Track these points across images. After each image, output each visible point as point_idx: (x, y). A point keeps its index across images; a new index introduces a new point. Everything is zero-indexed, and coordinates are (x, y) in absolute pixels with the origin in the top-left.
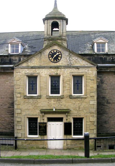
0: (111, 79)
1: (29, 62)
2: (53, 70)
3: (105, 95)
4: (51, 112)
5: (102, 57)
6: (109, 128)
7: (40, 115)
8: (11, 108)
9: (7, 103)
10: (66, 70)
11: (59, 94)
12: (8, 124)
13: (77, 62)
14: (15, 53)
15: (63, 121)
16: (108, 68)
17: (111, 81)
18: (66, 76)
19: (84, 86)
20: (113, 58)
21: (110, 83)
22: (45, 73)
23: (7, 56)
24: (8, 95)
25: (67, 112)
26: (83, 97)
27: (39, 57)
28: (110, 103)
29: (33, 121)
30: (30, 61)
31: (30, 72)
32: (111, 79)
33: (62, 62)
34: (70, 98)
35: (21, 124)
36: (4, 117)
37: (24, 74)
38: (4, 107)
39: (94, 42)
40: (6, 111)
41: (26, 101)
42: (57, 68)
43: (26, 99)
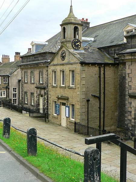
33: (66, 61)
42: (63, 65)
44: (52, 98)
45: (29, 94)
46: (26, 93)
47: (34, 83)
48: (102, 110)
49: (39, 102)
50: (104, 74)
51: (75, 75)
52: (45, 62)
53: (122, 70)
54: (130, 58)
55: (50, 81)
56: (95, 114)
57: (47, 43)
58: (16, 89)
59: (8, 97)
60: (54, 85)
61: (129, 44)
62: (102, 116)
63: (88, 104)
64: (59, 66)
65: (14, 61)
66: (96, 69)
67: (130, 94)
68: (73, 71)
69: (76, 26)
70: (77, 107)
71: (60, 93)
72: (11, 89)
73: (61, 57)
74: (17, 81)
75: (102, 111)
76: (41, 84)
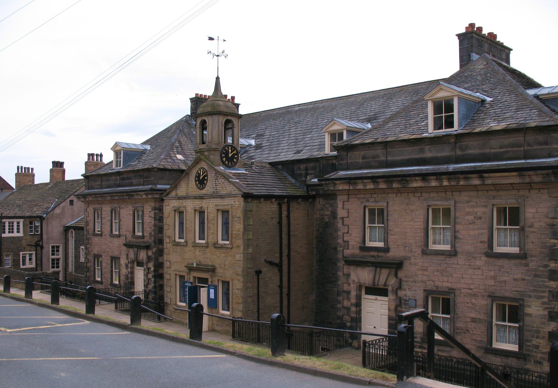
33: (209, 188)
34: (216, 247)
42: (201, 198)
44: (173, 269)
45: (106, 261)
46: (97, 257)
47: (119, 236)
48: (285, 291)
49: (133, 278)
50: (288, 217)
51: (230, 220)
52: (152, 190)
53: (322, 210)
54: (346, 187)
55: (168, 232)
56: (271, 299)
57: (148, 147)
58: (58, 247)
59: (39, 268)
60: (178, 240)
61: (343, 160)
62: (285, 302)
63: (258, 279)
64: (192, 200)
65: (48, 181)
66: (273, 207)
67: (345, 257)
68: (225, 213)
69: (229, 118)
70: (237, 286)
71: (194, 257)
72: (47, 249)
73: (196, 181)
74: (61, 229)
75: (285, 292)
76: (139, 237)
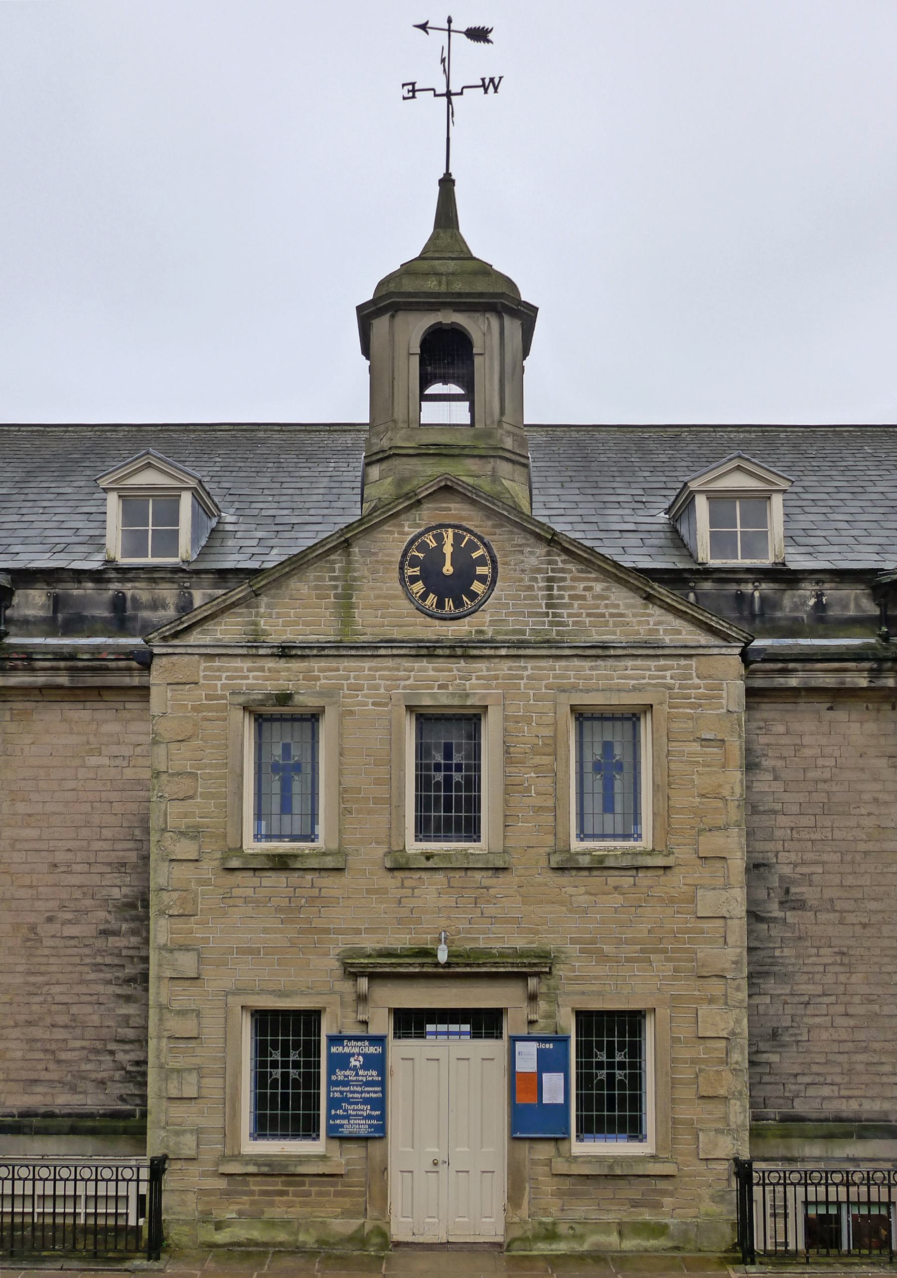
0: (807, 740)
1: (262, 610)
2: (432, 673)
3: (767, 848)
4: (420, 966)
5: (748, 588)
6: (800, 1079)
7: (342, 995)
8: (116, 933)
9: (88, 903)
10: (525, 668)
11: (478, 839)
12: (97, 1051)
13: (603, 616)
14: (150, 560)
15: (499, 1036)
16: (791, 665)
17: (807, 752)
18: (523, 712)
19: (656, 788)
20: (822, 595)
21: (804, 770)
22: (376, 688)
23: (97, 577)
24: (97, 845)
25: (530, 970)
26: (650, 861)
27: (333, 579)
28: (800, 905)
29: (285, 1033)
30: (269, 606)
31: (262, 678)
32: (807, 740)
35: (197, 1061)
36: (65, 999)
37: (223, 697)
38: (70, 931)
39: (693, 486)
40: (81, 956)
41: (236, 892)
42: (461, 650)
43: (239, 877)
